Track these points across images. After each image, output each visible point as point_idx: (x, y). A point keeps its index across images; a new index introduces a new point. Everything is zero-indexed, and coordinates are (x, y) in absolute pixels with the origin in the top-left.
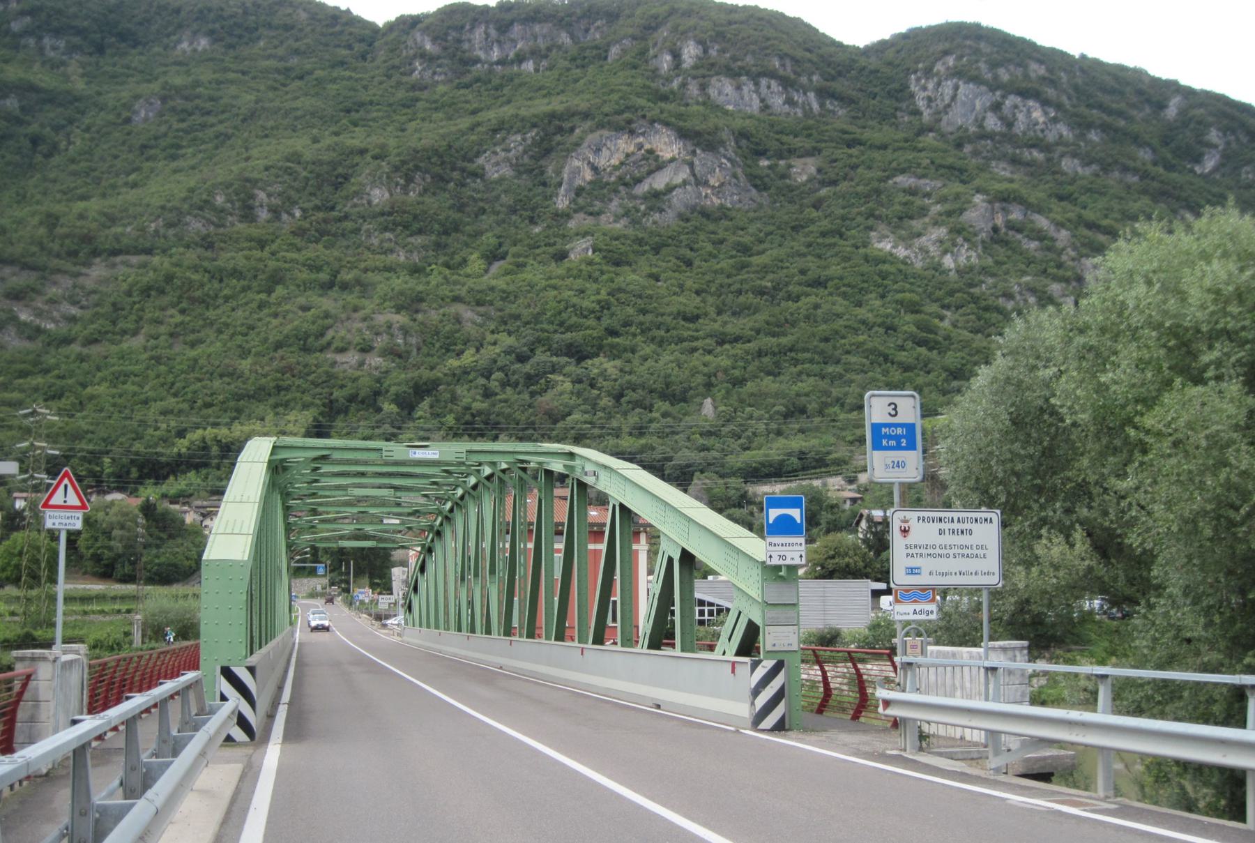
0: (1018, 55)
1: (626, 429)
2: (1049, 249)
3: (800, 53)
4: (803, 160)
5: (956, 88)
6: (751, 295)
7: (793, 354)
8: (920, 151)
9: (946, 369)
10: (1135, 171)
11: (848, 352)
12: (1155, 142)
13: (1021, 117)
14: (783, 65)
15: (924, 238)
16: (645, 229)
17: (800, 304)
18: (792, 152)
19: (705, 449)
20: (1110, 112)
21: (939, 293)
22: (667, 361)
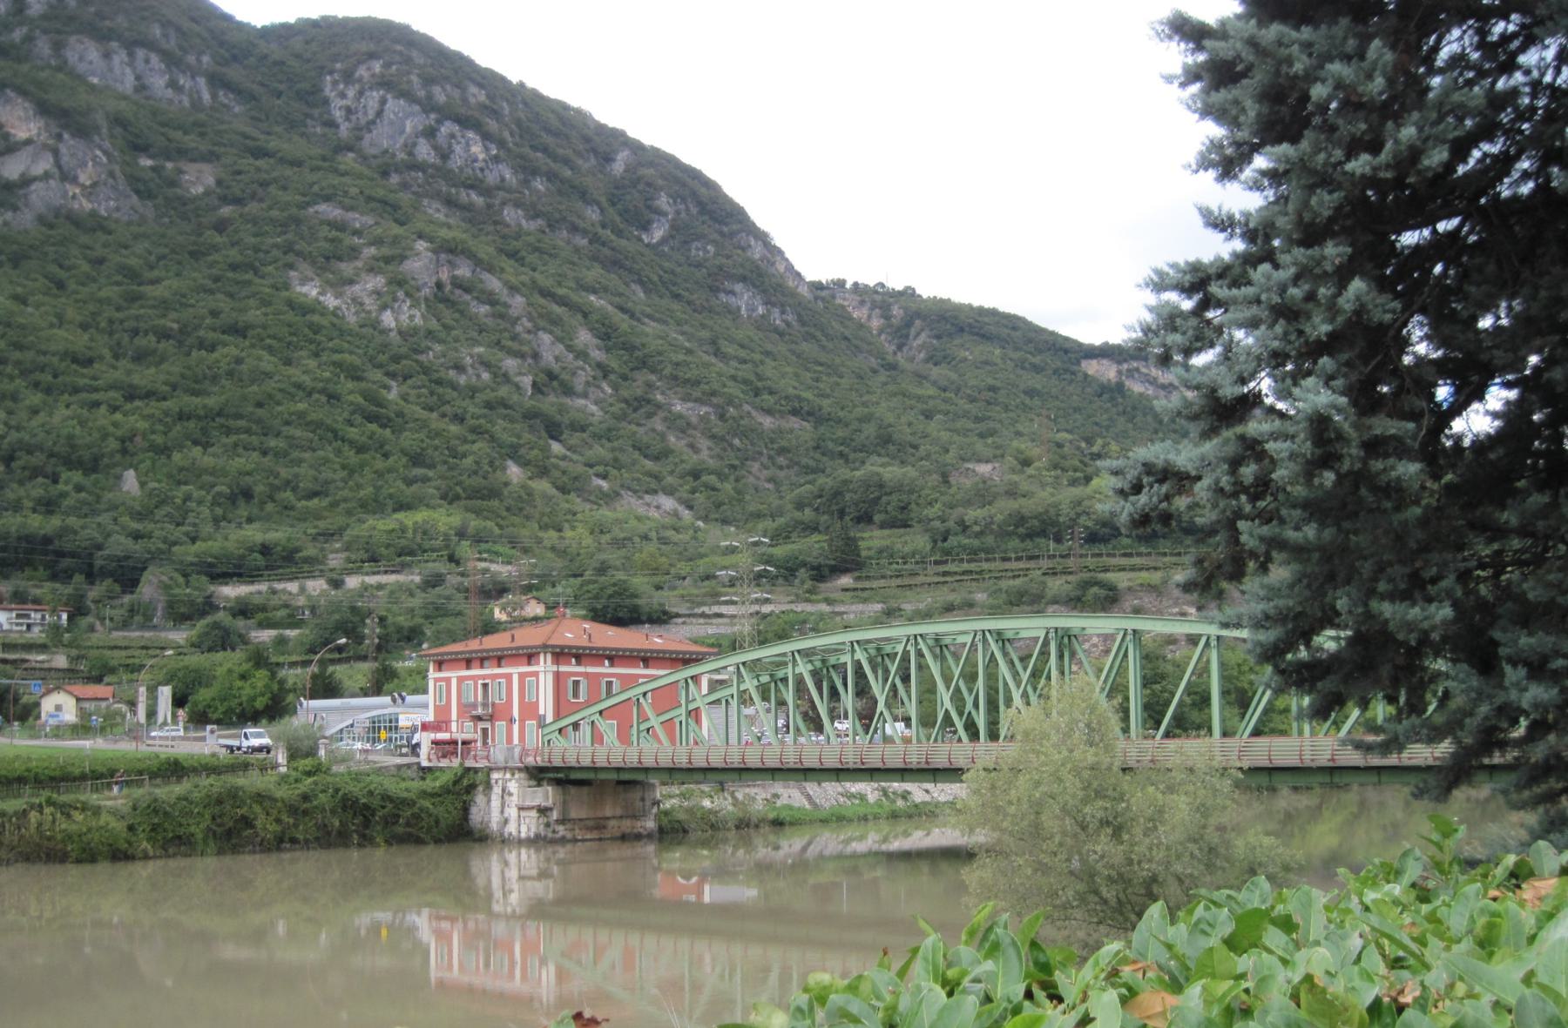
0: (456, 72)
1: (28, 504)
2: (502, 316)
3: (186, 24)
5: (383, 102)
6: (153, 339)
8: (342, 175)
9: (404, 452)
10: (585, 232)
11: (288, 423)
12: (603, 200)
13: (458, 149)
14: (165, 36)
15: (357, 288)
17: (215, 355)
18: (182, 153)
19: (137, 536)
20: (555, 157)
21: (382, 358)
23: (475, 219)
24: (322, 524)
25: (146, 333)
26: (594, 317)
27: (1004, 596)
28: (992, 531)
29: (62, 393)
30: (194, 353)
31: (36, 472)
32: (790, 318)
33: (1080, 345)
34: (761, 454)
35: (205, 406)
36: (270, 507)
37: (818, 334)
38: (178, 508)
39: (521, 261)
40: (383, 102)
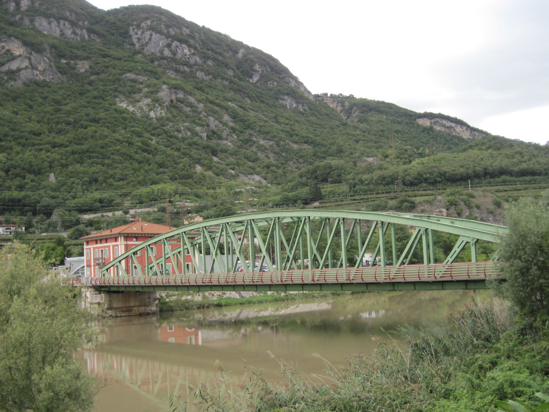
2: (195, 111)
4: (82, 62)
5: (151, 35)
6: (64, 125)
7: (88, 154)
8: (136, 62)
9: (157, 163)
10: (227, 79)
11: (113, 154)
12: (234, 67)
13: (179, 51)
14: (71, 15)
15: (141, 103)
16: (7, 89)
18: (77, 57)
19: (53, 197)
21: (150, 129)
22: (28, 155)
23: (189, 76)
24: (124, 191)
25: (62, 123)
26: (230, 110)
27: (371, 207)
28: (372, 183)
29: (29, 146)
30: (79, 130)
31: (17, 175)
32: (306, 108)
33: (416, 113)
34: (293, 158)
35: (82, 149)
36: (104, 185)
37: (316, 113)
38: (70, 186)
39: (203, 91)
40: (151, 35)
